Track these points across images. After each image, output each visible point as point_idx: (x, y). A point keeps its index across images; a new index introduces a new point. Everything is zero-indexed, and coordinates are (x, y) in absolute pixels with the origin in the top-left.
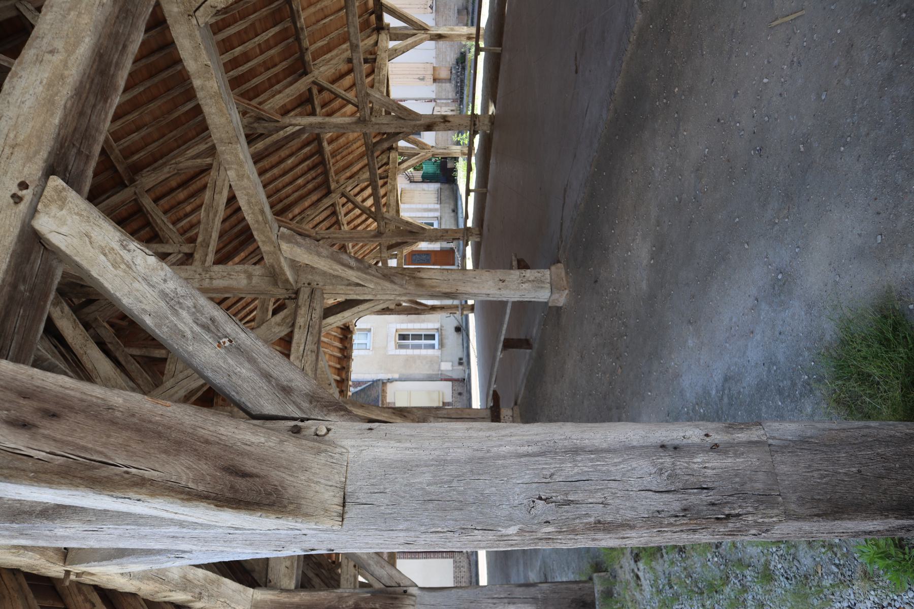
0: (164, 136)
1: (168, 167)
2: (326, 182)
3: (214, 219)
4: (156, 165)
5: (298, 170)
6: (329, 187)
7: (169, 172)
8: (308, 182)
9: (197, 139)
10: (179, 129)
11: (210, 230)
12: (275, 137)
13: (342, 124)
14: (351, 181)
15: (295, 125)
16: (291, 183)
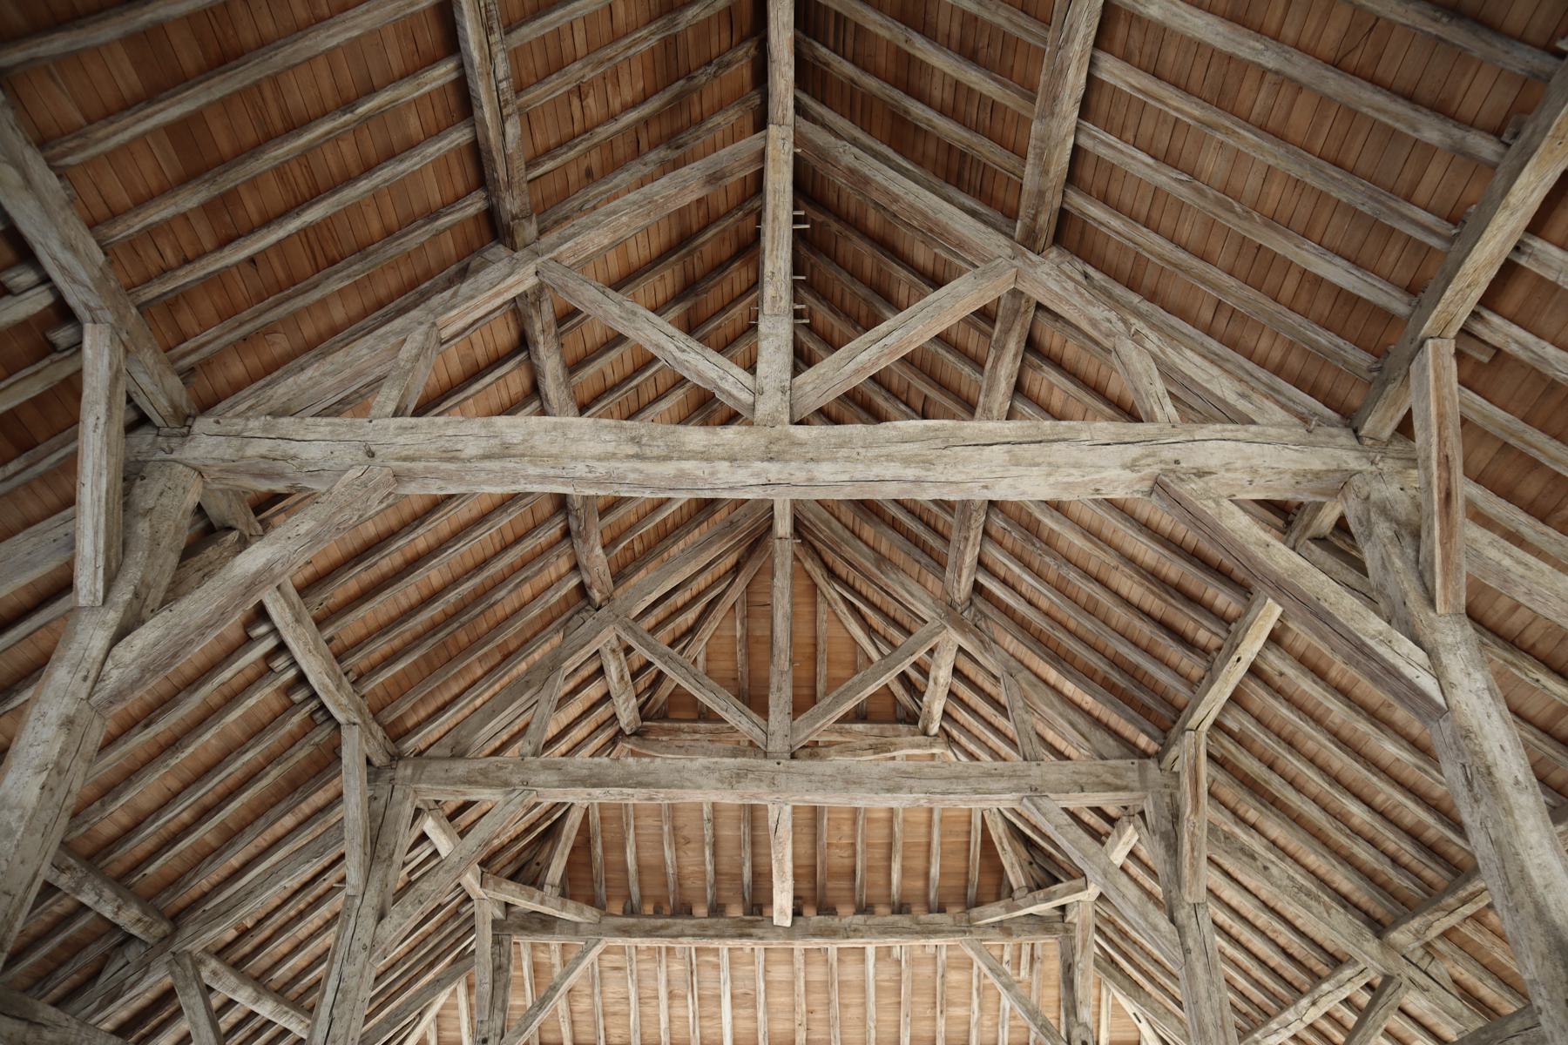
0: (1203, 257)
1: (1113, 316)
2: (1408, 908)
3: (890, 458)
4: (1119, 290)
5: (1388, 794)
6: (1396, 924)
7: (1093, 323)
8: (1372, 842)
9: (1263, 375)
10: (1251, 293)
11: (844, 452)
12: (1371, 626)
13: (1523, 875)
14: (1454, 1004)
15: (1437, 669)
16: (1336, 780)
